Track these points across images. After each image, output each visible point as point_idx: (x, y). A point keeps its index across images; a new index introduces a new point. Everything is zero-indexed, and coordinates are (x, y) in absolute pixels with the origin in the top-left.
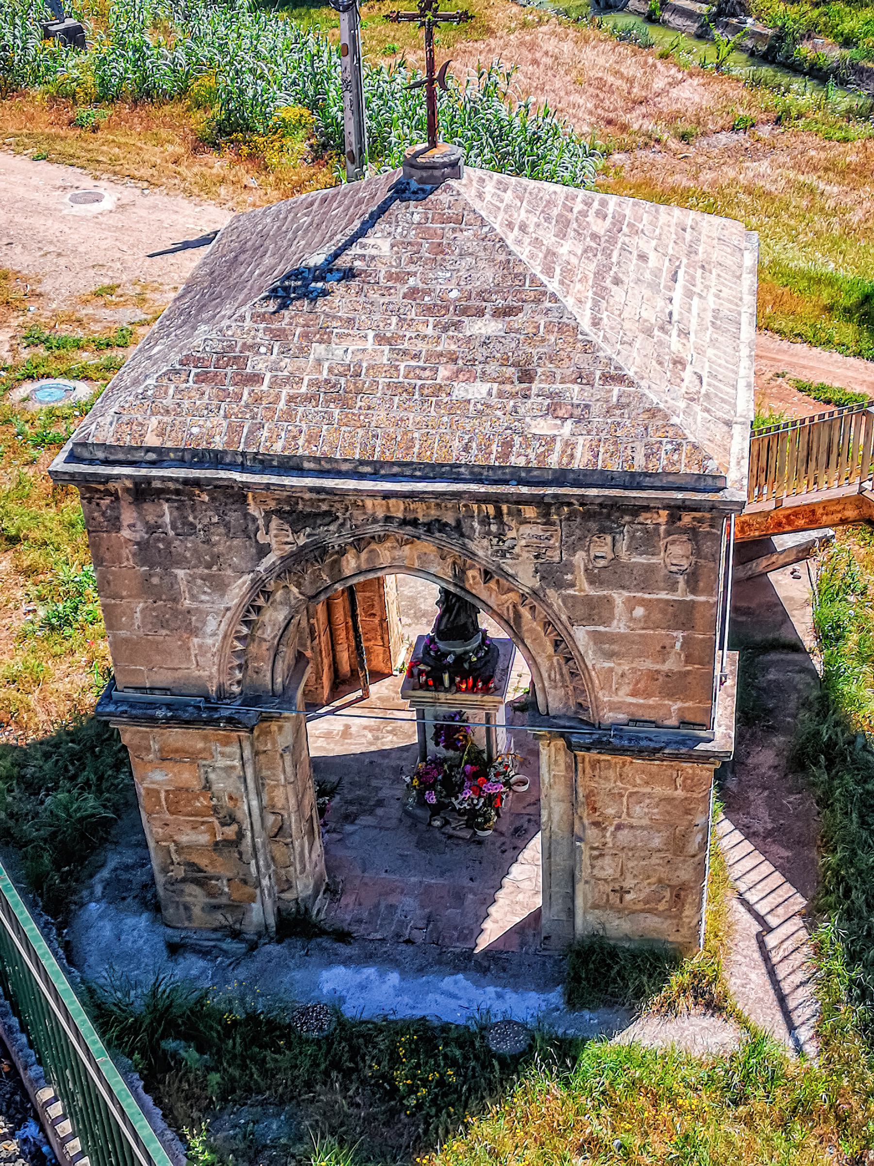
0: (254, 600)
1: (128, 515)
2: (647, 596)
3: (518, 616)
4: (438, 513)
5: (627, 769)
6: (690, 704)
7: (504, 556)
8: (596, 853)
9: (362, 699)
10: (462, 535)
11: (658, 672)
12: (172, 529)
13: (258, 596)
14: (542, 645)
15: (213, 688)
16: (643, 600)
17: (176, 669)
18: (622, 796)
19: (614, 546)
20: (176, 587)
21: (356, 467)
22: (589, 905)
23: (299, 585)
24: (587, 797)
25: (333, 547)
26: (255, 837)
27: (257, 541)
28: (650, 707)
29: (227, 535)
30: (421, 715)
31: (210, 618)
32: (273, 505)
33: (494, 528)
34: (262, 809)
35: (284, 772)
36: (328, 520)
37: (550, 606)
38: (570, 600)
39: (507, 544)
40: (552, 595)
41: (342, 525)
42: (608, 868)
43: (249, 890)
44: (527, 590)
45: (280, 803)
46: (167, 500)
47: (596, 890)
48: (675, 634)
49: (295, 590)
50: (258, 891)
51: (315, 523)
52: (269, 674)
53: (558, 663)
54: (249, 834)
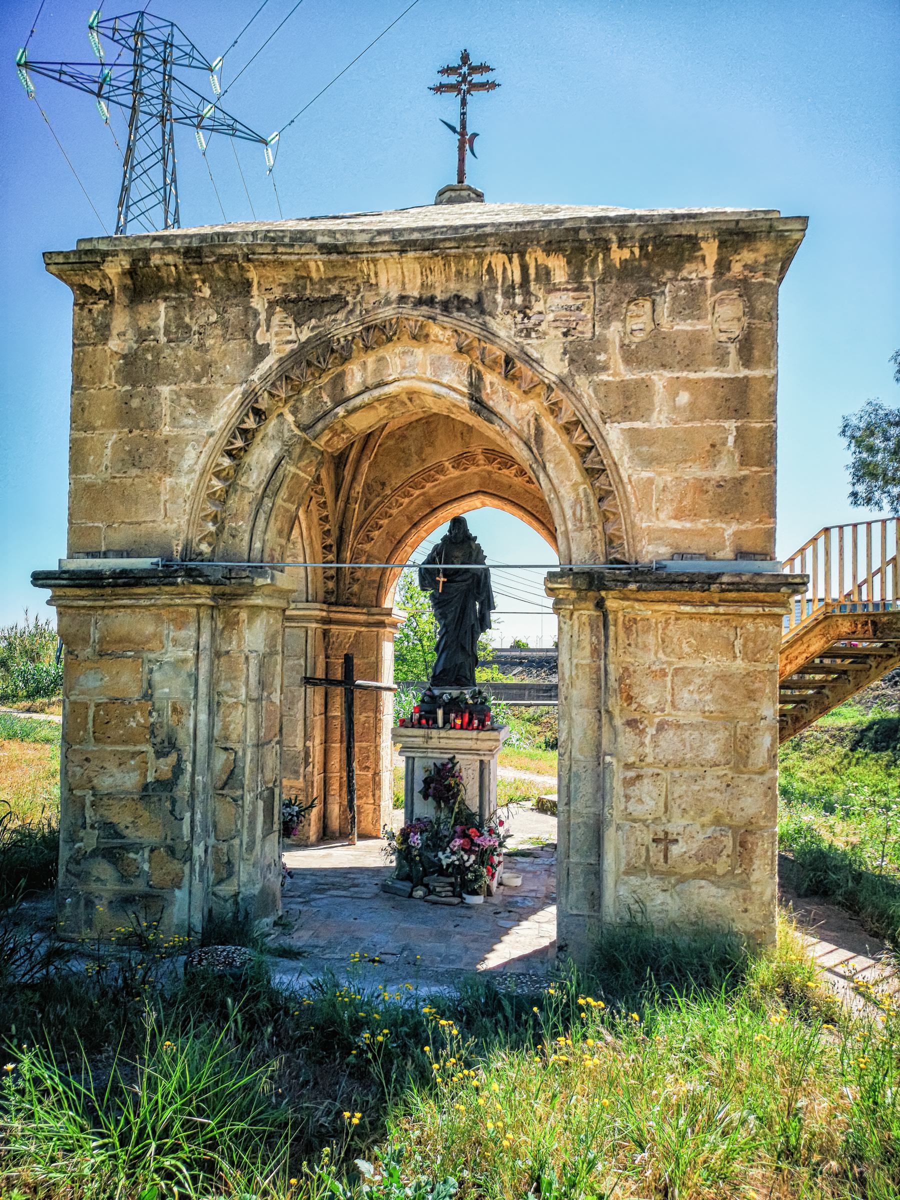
0: (243, 422)
1: (120, 320)
2: (692, 376)
3: (539, 432)
4: (458, 286)
6: (747, 525)
7: (528, 336)
8: (631, 774)
10: (483, 312)
11: (708, 480)
14: (567, 470)
16: (689, 381)
17: (139, 523)
18: (665, 675)
19: (654, 311)
20: (158, 409)
21: (373, 238)
22: (623, 868)
23: (295, 411)
24: (620, 680)
25: (338, 340)
26: (197, 778)
27: (255, 342)
28: (700, 533)
29: (223, 336)
30: (410, 761)
31: (189, 448)
32: (278, 293)
33: (519, 300)
34: (211, 739)
35: (247, 685)
36: (335, 307)
37: (579, 399)
38: (603, 388)
39: (533, 321)
40: (582, 383)
41: (351, 312)
43: (175, 866)
44: (554, 379)
45: (235, 730)
46: (165, 299)
47: (632, 840)
48: (726, 425)
49: (290, 418)
50: (187, 869)
51: (322, 312)
52: (247, 537)
53: (586, 495)
54: (189, 768)
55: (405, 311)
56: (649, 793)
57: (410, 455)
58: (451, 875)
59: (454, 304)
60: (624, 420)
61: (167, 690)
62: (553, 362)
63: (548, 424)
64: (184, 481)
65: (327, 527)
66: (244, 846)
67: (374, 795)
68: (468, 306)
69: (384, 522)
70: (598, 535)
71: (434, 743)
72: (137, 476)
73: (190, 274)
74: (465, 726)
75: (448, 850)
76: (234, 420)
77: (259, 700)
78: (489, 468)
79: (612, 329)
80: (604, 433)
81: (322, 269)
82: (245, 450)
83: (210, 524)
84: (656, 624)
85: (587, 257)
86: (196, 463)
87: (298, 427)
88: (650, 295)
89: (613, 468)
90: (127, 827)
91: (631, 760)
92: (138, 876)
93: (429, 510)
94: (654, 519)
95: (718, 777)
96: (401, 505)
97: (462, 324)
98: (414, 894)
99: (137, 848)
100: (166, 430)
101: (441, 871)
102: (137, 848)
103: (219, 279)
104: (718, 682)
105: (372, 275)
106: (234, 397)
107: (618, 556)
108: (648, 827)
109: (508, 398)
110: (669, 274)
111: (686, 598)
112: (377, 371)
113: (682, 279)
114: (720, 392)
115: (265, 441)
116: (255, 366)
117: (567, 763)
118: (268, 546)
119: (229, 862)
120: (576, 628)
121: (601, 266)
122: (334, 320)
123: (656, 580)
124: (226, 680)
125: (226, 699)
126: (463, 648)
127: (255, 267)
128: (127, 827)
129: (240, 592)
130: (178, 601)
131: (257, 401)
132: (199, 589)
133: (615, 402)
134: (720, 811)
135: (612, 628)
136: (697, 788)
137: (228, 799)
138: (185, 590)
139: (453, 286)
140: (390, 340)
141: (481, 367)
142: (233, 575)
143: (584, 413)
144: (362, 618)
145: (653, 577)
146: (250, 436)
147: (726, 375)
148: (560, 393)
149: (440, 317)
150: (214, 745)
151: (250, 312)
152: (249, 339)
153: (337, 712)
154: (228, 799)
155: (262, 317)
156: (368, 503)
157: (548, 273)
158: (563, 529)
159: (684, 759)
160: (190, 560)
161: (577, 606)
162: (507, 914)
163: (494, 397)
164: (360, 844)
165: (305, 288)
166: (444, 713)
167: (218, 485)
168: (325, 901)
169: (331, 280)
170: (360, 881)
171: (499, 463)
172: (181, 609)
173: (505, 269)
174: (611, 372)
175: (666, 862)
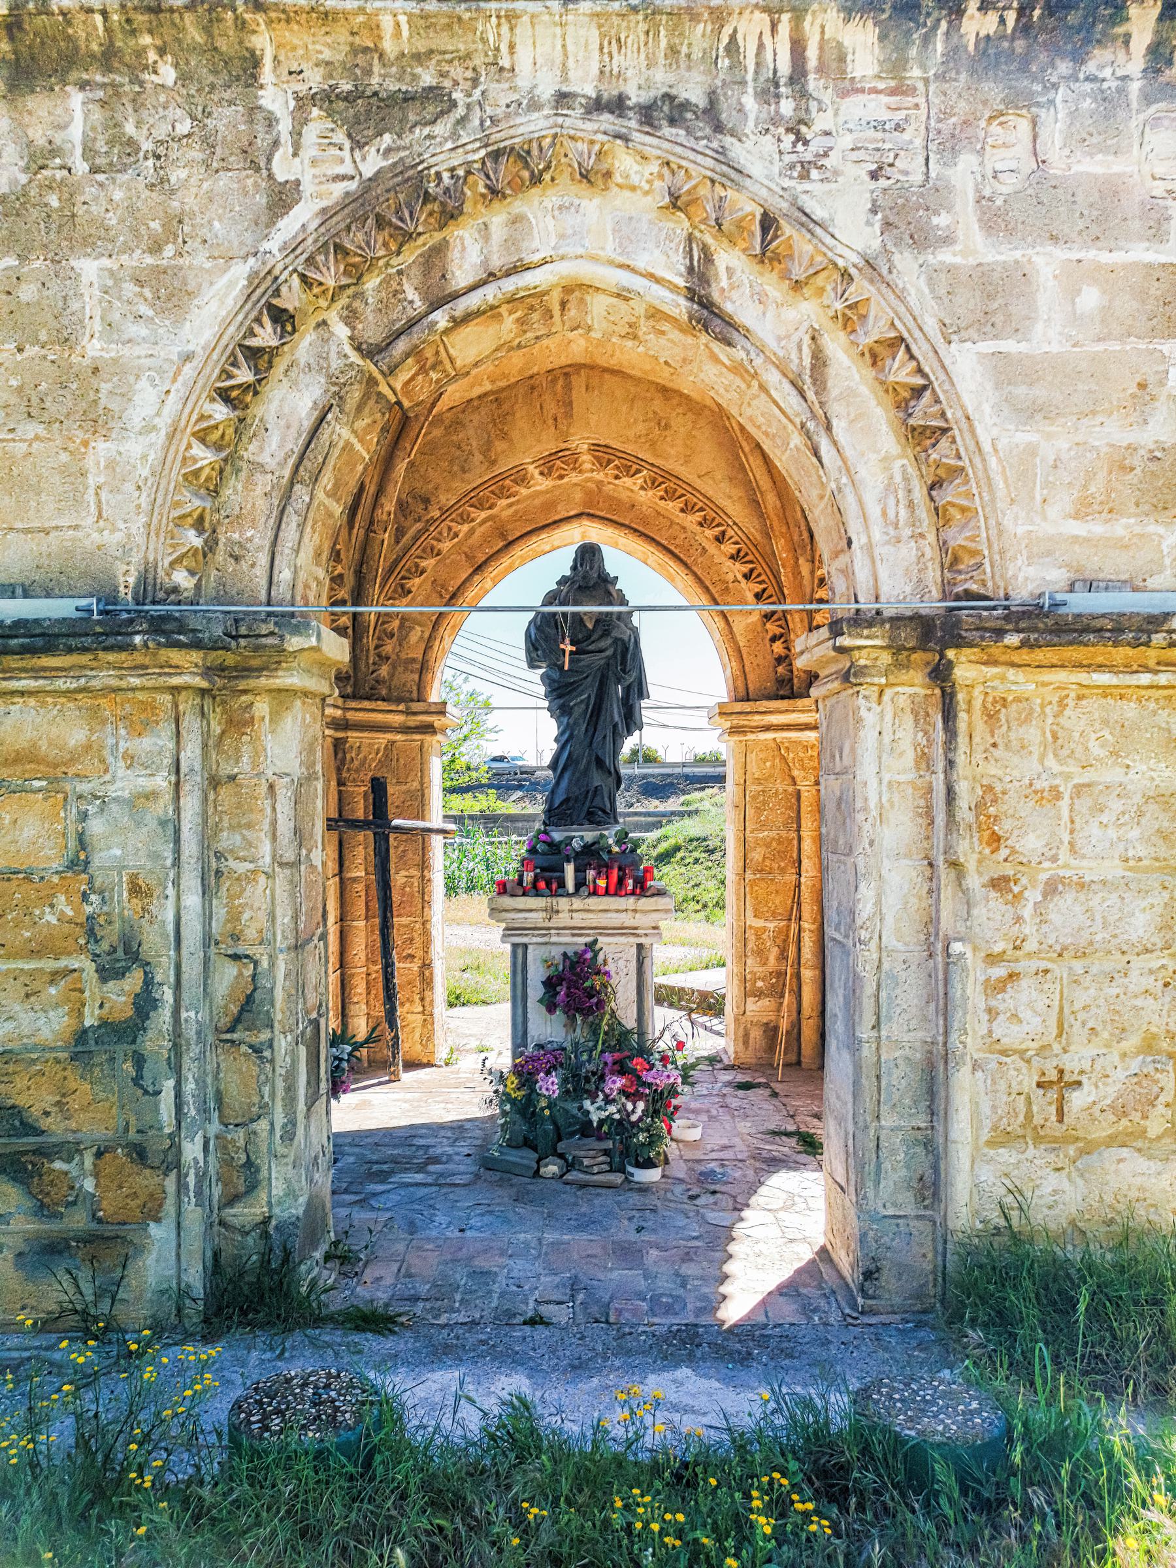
0: (251, 333)
2: (1105, 257)
3: (819, 361)
4: (671, 78)
5: (1073, 719)
8: (1000, 972)
9: (390, 1081)
10: (719, 128)
11: (1132, 448)
12: (85, 158)
13: (258, 320)
15: (127, 580)
16: (1099, 267)
18: (1058, 796)
19: (1035, 138)
20: (75, 305)
22: (985, 1135)
23: (351, 317)
25: (438, 174)
26: (192, 1005)
27: (270, 176)
30: (520, 953)
31: (143, 383)
32: (315, 80)
33: (787, 107)
34: (208, 940)
35: (274, 838)
36: (431, 109)
41: (462, 121)
42: (1028, 1014)
43: (147, 1180)
44: (855, 258)
46: (83, 85)
47: (1002, 1086)
49: (342, 331)
50: (170, 1183)
51: (403, 120)
52: (263, 559)
53: (906, 479)
54: (168, 995)
55: (568, 122)
56: (1030, 1005)
57: (471, 453)
58: (608, 1136)
59: (665, 111)
60: (984, 336)
61: (118, 852)
62: (854, 232)
63: (836, 346)
64: (134, 447)
65: (339, 570)
66: (278, 1133)
67: (422, 999)
68: (689, 115)
69: (429, 563)
70: (928, 550)
71: (563, 919)
72: (37, 438)
73: (133, 32)
74: (612, 889)
75: (601, 1096)
76: (232, 329)
77: (295, 864)
78: (599, 476)
79: (961, 166)
80: (947, 362)
81: (405, 33)
82: (253, 388)
83: (192, 533)
84: (1042, 706)
85: (918, 26)
86: (158, 414)
87: (358, 349)
88: (1028, 107)
89: (964, 424)
90: (47, 1114)
91: (997, 948)
92: (74, 1203)
93: (501, 544)
94: (1038, 520)
95: (1151, 972)
96: (456, 535)
97: (678, 149)
98: (542, 1170)
99: (69, 1150)
100: (94, 348)
101: (586, 1129)
102: (69, 1150)
103: (194, 48)
104: (1152, 807)
105: (504, 48)
106: (231, 284)
107: (974, 587)
108: (1028, 1061)
109: (761, 299)
110: (1064, 67)
111: (1100, 659)
112: (511, 243)
113: (1087, 79)
114: (1155, 290)
115: (293, 374)
116: (271, 223)
117: (875, 956)
118: (302, 575)
119: (249, 1163)
120: (889, 717)
121: (940, 47)
122: (428, 137)
123: (1047, 627)
124: (232, 828)
125: (232, 863)
126: (600, 763)
127: (269, 23)
128: (47, 1114)
129: (255, 663)
130: (135, 681)
131: (277, 293)
132: (175, 656)
133: (967, 303)
134: (1154, 1029)
135: (963, 716)
136: (1114, 991)
137: (244, 1048)
138: (147, 661)
139: (662, 79)
140: (536, 180)
141: (709, 240)
142: (243, 630)
143: (911, 324)
144: (398, 719)
145: (1050, 622)
146: (262, 364)
147: (1163, 259)
148: (866, 284)
149: (637, 136)
150: (213, 950)
151: (259, 116)
152: (258, 169)
153: (359, 870)
154: (244, 1048)
155: (285, 126)
156: (400, 533)
157: (842, 59)
158: (864, 540)
159: (1091, 943)
160: (154, 603)
161: (892, 679)
162: (711, 1199)
163: (734, 295)
164: (407, 1077)
165: (368, 73)
166: (577, 870)
167: (204, 456)
168: (394, 1197)
169: (419, 58)
170: (439, 1151)
171: (617, 467)
172: (141, 696)
173: (761, 46)
174: (958, 247)
175: (1061, 1121)
